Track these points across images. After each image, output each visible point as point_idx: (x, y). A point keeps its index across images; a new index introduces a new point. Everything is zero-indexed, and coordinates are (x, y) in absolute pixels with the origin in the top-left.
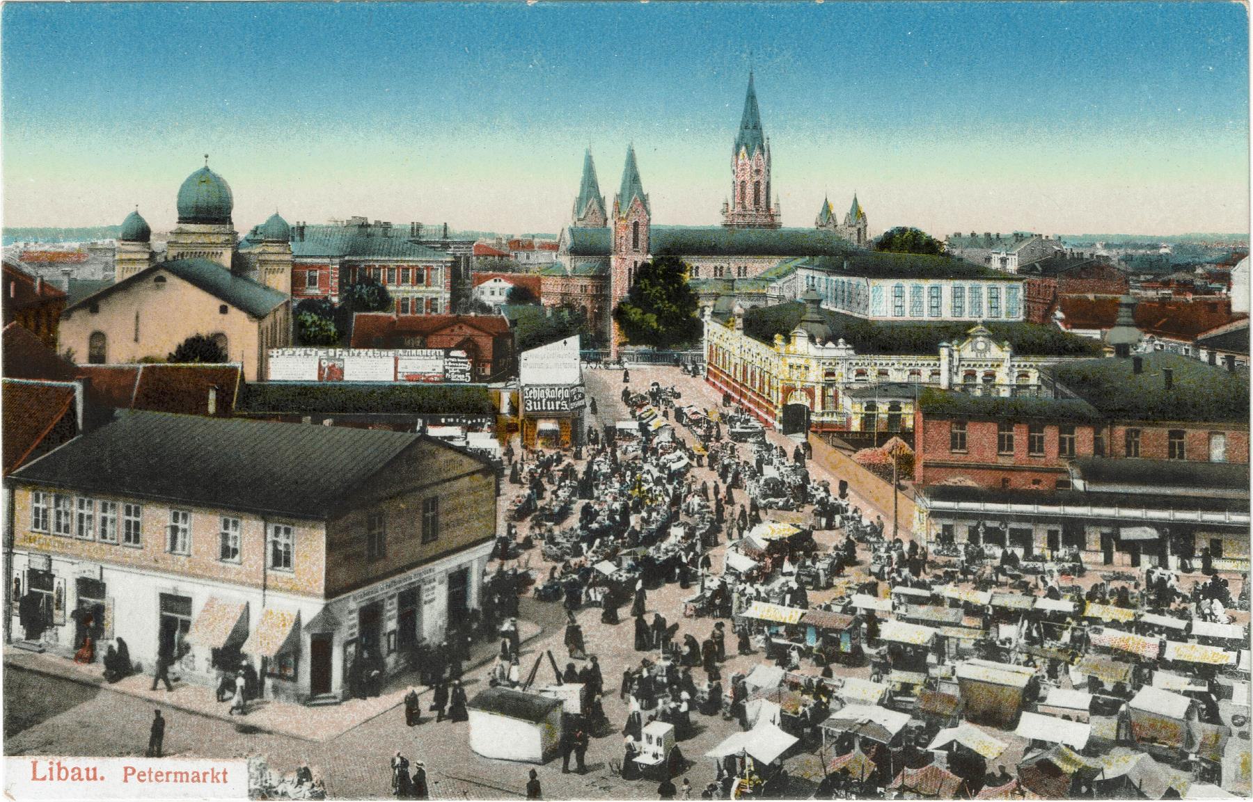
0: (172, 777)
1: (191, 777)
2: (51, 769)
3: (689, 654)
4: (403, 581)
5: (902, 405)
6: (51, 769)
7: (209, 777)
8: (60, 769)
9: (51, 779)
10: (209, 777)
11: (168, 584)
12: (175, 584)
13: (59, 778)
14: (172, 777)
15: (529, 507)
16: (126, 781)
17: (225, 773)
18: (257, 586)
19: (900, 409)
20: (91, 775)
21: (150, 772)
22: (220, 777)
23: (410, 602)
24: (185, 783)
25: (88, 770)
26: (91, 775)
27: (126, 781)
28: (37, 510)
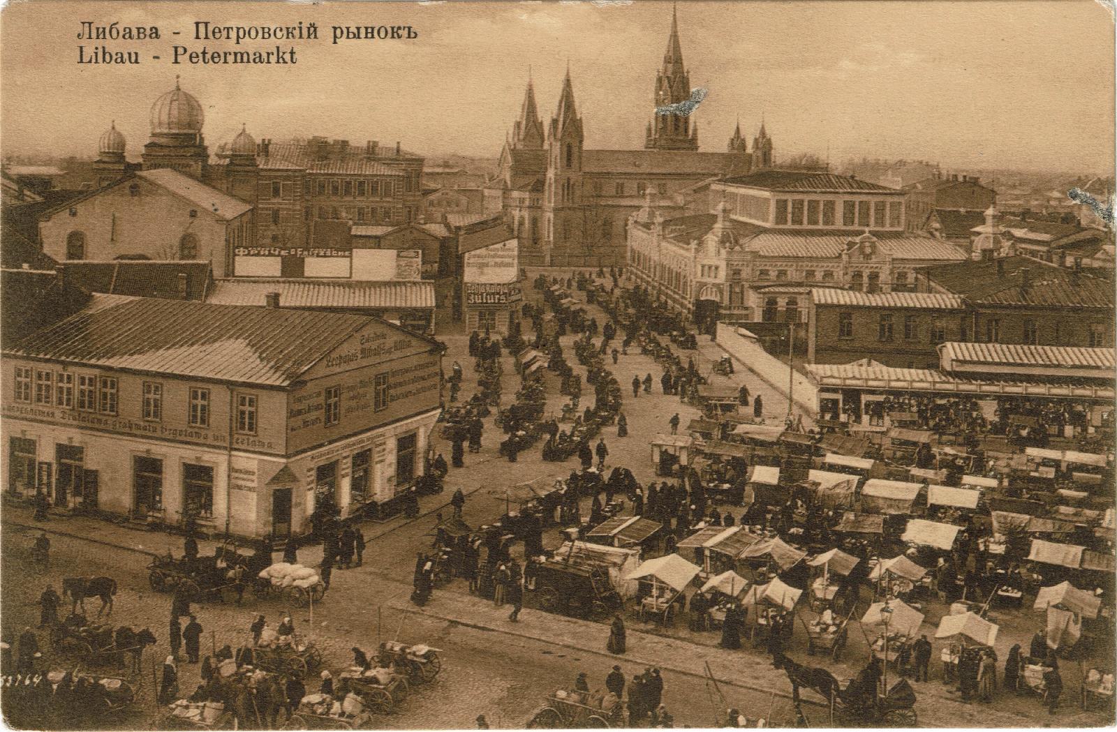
0: (231, 58)
1: (252, 57)
2: (96, 53)
3: (1102, 588)
4: (402, 427)
5: (799, 301)
6: (96, 53)
7: (273, 58)
8: (104, 53)
9: (96, 62)
10: (273, 58)
11: (142, 447)
12: (145, 447)
13: (104, 61)
14: (231, 58)
15: (1013, 492)
16: (335, 42)
17: (292, 53)
18: (225, 448)
19: (797, 304)
20: (133, 59)
21: (204, 53)
22: (287, 57)
23: (363, 460)
24: (240, 65)
25: (130, 54)
26: (133, 59)
27: (335, 42)
28: (243, 413)
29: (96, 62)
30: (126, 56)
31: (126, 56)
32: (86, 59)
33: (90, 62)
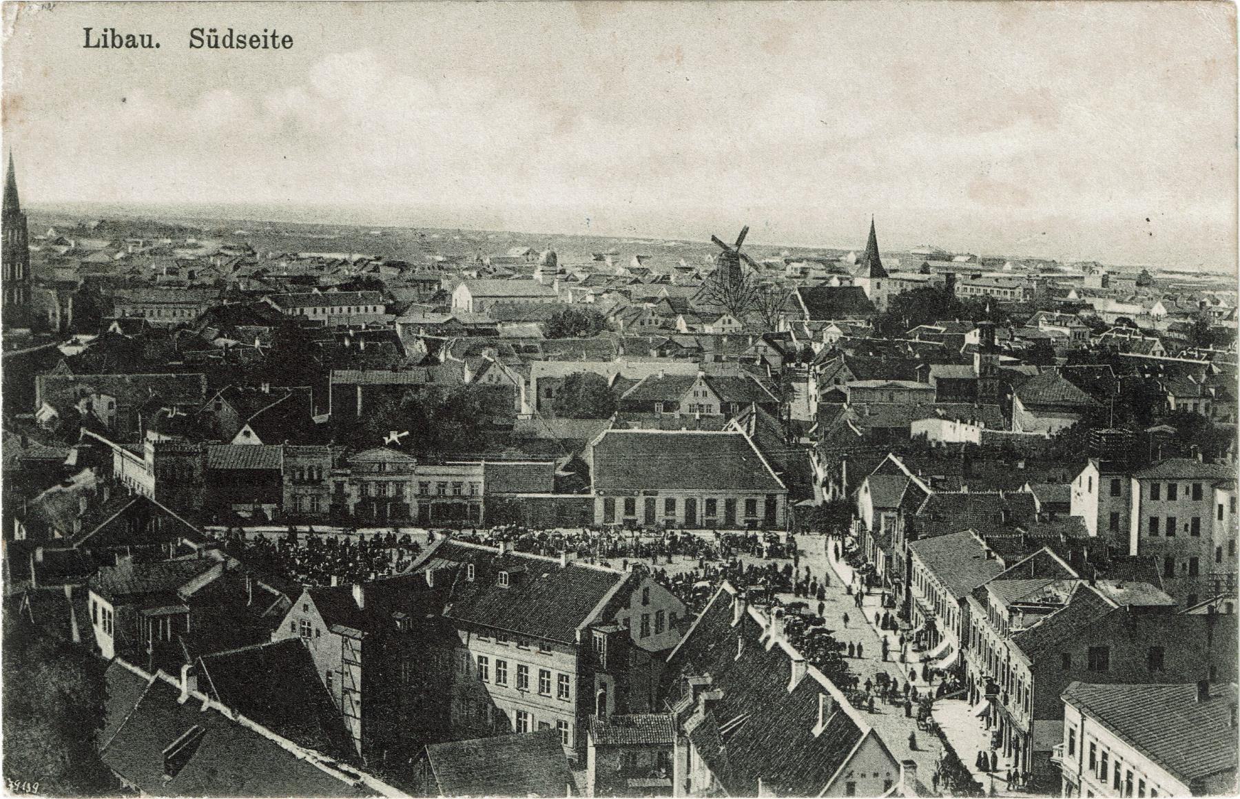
25: (143, 36)
29: (105, 46)
30: (138, 40)
31: (138, 40)
32: (93, 42)
33: (98, 46)
